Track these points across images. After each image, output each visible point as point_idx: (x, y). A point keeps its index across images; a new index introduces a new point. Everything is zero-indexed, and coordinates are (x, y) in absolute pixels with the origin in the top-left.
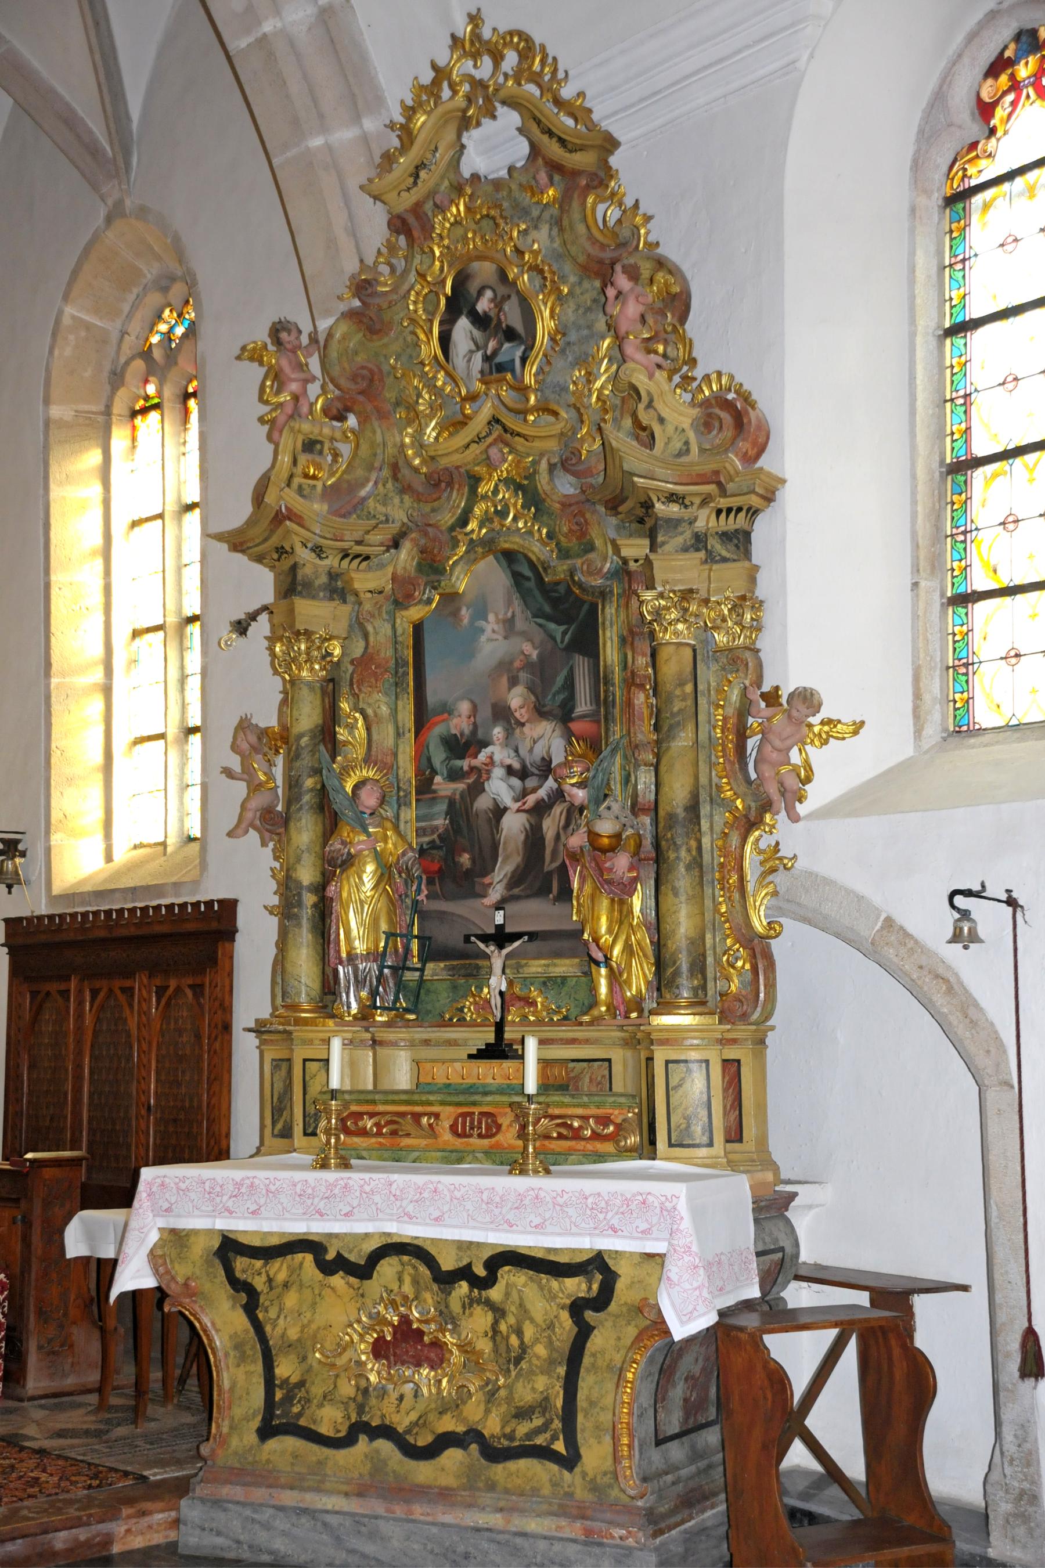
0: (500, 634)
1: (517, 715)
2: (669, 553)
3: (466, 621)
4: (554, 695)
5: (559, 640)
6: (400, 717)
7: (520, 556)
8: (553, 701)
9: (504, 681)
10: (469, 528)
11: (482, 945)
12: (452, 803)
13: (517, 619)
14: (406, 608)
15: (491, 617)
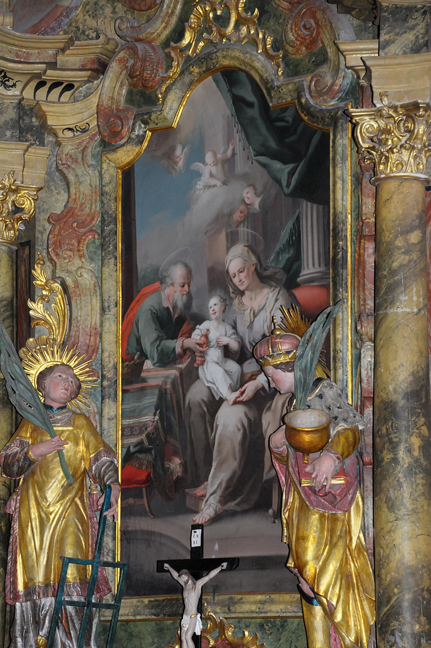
0: (217, 180)
1: (236, 281)
2: (396, 56)
3: (181, 164)
4: (278, 254)
5: (284, 183)
6: (105, 287)
7: (243, 76)
8: (276, 264)
9: (222, 237)
10: (186, 41)
11: (175, 574)
12: (162, 394)
13: (238, 158)
14: (115, 149)
15: (209, 157)
